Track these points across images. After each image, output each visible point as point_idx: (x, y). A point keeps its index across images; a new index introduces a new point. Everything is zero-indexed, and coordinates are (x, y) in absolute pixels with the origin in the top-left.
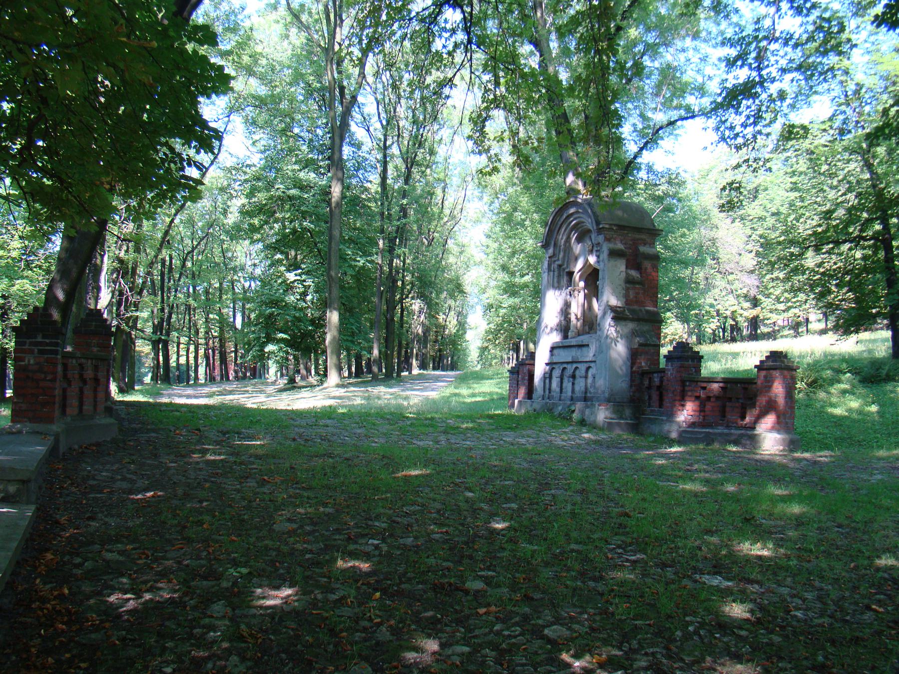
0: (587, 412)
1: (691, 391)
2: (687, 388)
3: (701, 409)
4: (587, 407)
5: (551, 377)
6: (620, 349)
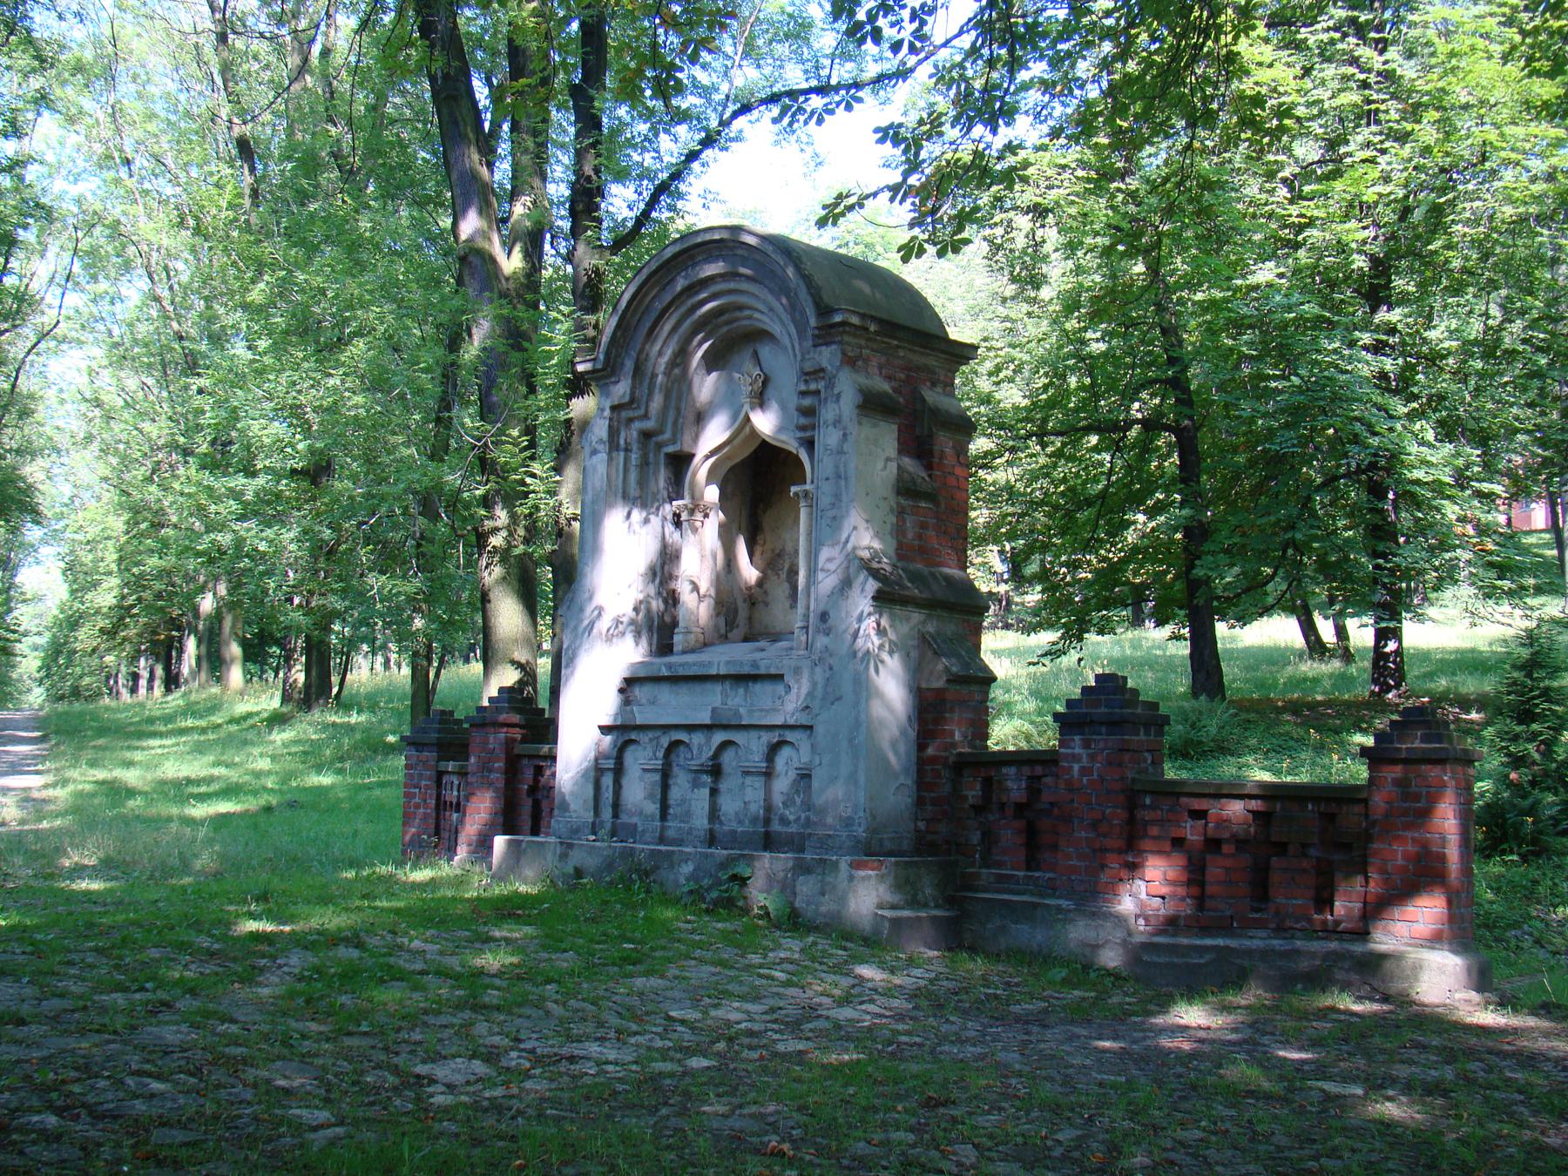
0: (806, 886)
1: (1160, 822)
3: (1195, 877)
4: (803, 868)
5: (619, 771)
6: (891, 687)
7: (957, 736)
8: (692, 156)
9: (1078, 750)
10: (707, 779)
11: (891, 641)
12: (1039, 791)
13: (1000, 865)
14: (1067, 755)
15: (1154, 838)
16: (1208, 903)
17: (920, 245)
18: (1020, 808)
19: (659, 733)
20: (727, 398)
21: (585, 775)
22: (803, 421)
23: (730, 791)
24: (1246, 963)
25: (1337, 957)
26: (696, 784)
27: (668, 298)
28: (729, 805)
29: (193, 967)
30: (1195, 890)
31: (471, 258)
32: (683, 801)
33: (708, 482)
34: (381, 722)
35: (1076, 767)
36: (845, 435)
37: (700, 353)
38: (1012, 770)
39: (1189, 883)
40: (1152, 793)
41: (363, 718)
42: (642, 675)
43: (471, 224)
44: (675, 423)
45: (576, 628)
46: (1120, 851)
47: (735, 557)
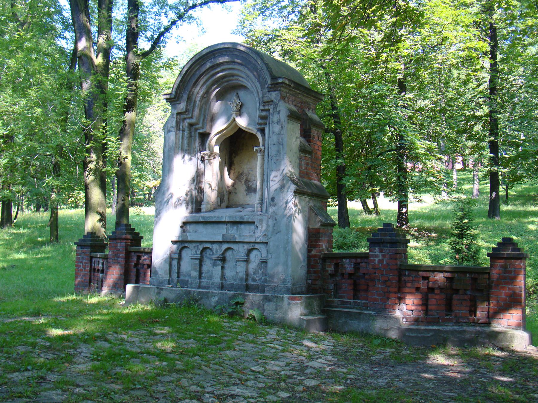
0: (269, 307)
1: (412, 282)
2: (403, 278)
3: (425, 304)
4: (267, 299)
5: (180, 259)
7: (324, 247)
8: (174, 23)
9: (377, 253)
10: (220, 263)
11: (299, 209)
12: (359, 269)
13: (341, 297)
14: (372, 255)
15: (409, 287)
16: (430, 313)
17: (329, 50)
18: (350, 275)
19: (198, 244)
20: (226, 112)
21: (165, 261)
22: (261, 121)
23: (229, 267)
24: (446, 336)
25: (479, 333)
26: (215, 265)
27: (203, 70)
28: (229, 273)
29: (42, 355)
30: (424, 308)
31: (83, 57)
32: (209, 271)
33: (215, 145)
34: (33, 233)
35: (377, 260)
36: (282, 127)
37: (214, 93)
38: (347, 260)
39: (423, 304)
40: (408, 270)
41: (25, 231)
42: (191, 221)
43: (82, 44)
44: (204, 120)
45: (161, 202)
46: (395, 293)
47: (224, 174)
